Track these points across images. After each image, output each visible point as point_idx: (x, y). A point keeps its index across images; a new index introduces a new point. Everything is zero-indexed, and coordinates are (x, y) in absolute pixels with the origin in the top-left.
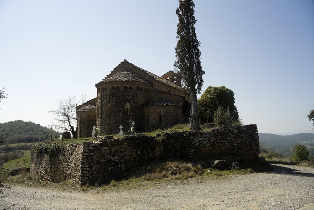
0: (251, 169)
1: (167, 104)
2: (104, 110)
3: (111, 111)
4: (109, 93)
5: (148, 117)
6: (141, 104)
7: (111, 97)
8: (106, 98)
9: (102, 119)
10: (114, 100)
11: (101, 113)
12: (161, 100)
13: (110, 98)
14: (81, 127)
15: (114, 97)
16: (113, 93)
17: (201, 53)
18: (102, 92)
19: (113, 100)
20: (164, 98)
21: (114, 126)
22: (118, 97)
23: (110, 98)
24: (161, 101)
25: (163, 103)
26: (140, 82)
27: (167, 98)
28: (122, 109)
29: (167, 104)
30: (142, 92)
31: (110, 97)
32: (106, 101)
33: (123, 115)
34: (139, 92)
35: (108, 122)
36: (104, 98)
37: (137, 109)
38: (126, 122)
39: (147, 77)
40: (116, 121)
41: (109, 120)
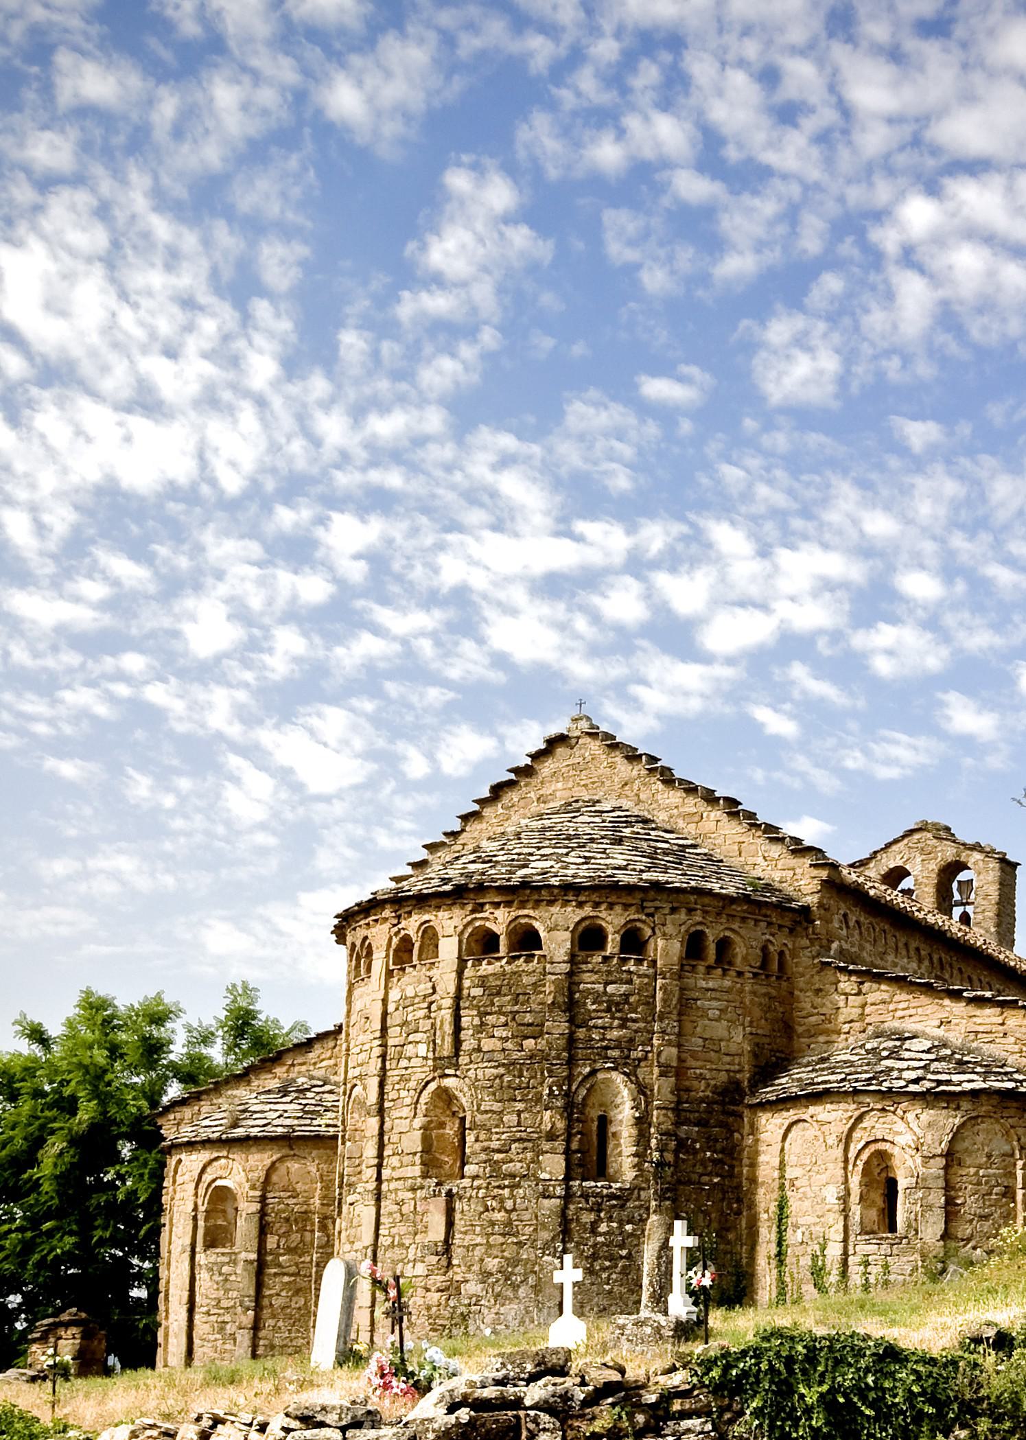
0: (520, 437)
1: (948, 1082)
2: (403, 1125)
3: (470, 1138)
4: (447, 984)
5: (782, 1187)
6: (723, 1077)
7: (465, 1022)
8: (425, 1025)
9: (387, 1206)
10: (498, 1045)
11: (380, 1156)
12: (891, 1044)
13: (458, 1029)
14: (203, 1276)
15: (490, 1019)
16: (483, 981)
17: (40, 1024)
18: (389, 974)
19: (487, 1044)
20: (918, 1027)
21: (492, 1264)
22: (529, 1018)
23: (458, 1029)
24: (894, 1054)
25: (913, 1075)
26: (710, 892)
27: (940, 1032)
28: (561, 1125)
29: (948, 1082)
30: (727, 983)
31: (457, 1018)
32: (422, 1050)
33: (568, 1167)
34: (703, 984)
35: (437, 1233)
36: (405, 1023)
37: (687, 1122)
38: (594, 1232)
39: (855, 758)
40: (509, 1223)
41: (450, 1212)
